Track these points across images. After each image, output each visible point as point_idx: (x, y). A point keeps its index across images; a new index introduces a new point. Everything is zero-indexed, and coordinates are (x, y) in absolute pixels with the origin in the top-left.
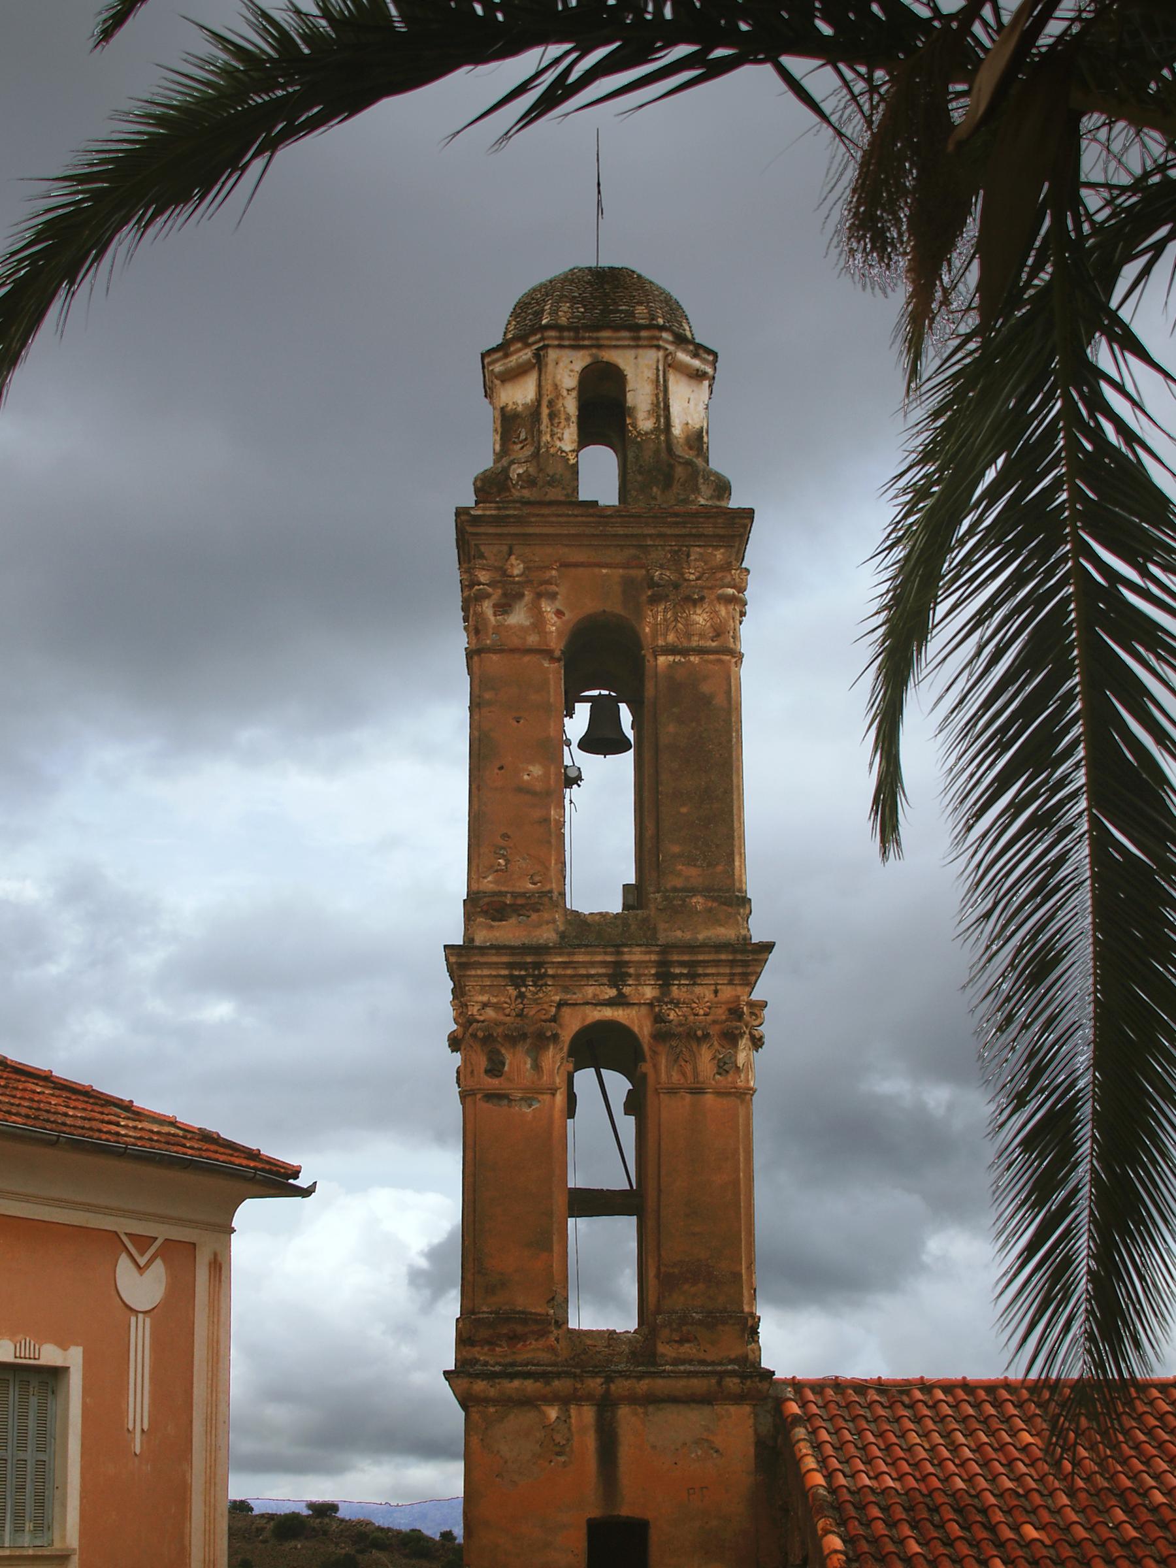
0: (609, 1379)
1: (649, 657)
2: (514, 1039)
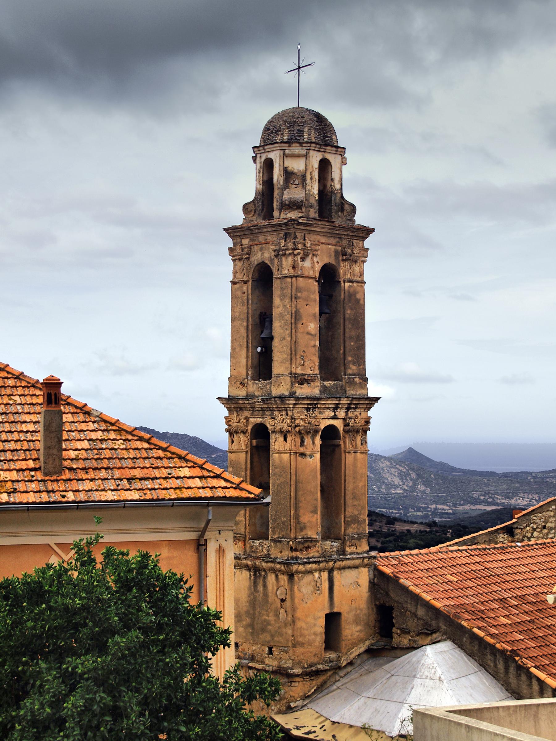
0: (335, 562)
1: (342, 282)
2: (308, 433)
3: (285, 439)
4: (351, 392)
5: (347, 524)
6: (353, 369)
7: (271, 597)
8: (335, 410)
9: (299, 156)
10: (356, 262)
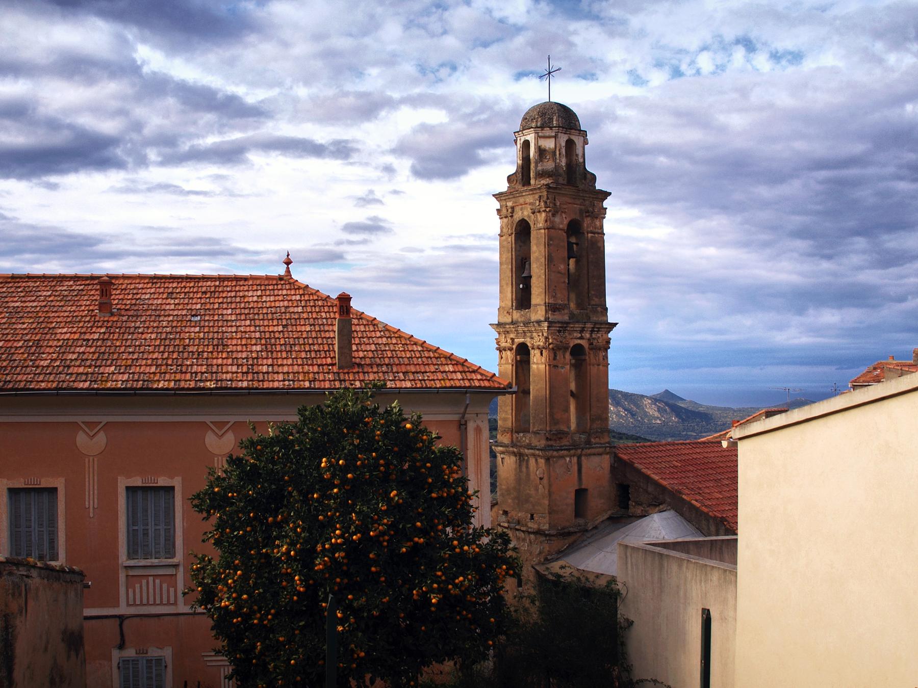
2: (559, 349)
3: (542, 354)
4: (594, 319)
5: (592, 421)
6: (596, 301)
7: (532, 477)
8: (581, 332)
9: (549, 137)
10: (597, 218)
